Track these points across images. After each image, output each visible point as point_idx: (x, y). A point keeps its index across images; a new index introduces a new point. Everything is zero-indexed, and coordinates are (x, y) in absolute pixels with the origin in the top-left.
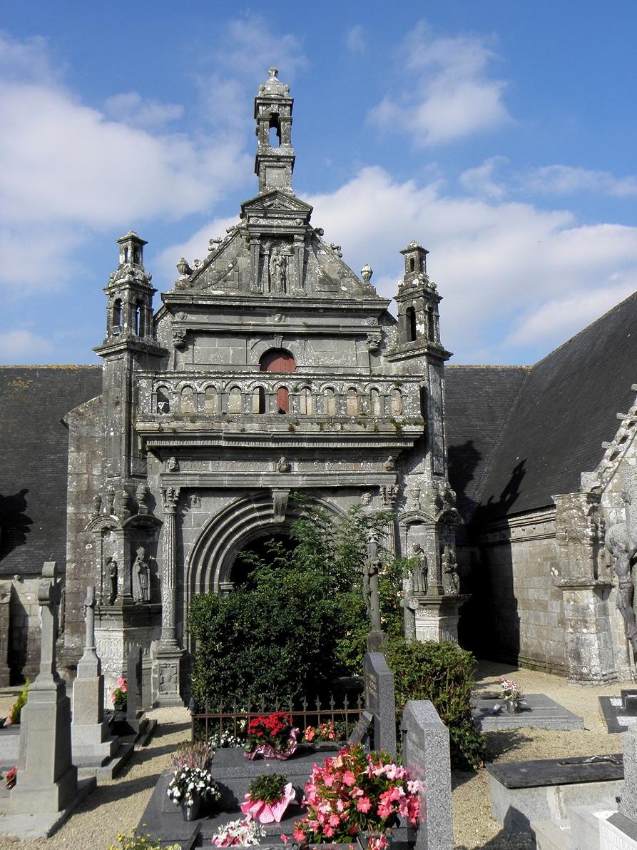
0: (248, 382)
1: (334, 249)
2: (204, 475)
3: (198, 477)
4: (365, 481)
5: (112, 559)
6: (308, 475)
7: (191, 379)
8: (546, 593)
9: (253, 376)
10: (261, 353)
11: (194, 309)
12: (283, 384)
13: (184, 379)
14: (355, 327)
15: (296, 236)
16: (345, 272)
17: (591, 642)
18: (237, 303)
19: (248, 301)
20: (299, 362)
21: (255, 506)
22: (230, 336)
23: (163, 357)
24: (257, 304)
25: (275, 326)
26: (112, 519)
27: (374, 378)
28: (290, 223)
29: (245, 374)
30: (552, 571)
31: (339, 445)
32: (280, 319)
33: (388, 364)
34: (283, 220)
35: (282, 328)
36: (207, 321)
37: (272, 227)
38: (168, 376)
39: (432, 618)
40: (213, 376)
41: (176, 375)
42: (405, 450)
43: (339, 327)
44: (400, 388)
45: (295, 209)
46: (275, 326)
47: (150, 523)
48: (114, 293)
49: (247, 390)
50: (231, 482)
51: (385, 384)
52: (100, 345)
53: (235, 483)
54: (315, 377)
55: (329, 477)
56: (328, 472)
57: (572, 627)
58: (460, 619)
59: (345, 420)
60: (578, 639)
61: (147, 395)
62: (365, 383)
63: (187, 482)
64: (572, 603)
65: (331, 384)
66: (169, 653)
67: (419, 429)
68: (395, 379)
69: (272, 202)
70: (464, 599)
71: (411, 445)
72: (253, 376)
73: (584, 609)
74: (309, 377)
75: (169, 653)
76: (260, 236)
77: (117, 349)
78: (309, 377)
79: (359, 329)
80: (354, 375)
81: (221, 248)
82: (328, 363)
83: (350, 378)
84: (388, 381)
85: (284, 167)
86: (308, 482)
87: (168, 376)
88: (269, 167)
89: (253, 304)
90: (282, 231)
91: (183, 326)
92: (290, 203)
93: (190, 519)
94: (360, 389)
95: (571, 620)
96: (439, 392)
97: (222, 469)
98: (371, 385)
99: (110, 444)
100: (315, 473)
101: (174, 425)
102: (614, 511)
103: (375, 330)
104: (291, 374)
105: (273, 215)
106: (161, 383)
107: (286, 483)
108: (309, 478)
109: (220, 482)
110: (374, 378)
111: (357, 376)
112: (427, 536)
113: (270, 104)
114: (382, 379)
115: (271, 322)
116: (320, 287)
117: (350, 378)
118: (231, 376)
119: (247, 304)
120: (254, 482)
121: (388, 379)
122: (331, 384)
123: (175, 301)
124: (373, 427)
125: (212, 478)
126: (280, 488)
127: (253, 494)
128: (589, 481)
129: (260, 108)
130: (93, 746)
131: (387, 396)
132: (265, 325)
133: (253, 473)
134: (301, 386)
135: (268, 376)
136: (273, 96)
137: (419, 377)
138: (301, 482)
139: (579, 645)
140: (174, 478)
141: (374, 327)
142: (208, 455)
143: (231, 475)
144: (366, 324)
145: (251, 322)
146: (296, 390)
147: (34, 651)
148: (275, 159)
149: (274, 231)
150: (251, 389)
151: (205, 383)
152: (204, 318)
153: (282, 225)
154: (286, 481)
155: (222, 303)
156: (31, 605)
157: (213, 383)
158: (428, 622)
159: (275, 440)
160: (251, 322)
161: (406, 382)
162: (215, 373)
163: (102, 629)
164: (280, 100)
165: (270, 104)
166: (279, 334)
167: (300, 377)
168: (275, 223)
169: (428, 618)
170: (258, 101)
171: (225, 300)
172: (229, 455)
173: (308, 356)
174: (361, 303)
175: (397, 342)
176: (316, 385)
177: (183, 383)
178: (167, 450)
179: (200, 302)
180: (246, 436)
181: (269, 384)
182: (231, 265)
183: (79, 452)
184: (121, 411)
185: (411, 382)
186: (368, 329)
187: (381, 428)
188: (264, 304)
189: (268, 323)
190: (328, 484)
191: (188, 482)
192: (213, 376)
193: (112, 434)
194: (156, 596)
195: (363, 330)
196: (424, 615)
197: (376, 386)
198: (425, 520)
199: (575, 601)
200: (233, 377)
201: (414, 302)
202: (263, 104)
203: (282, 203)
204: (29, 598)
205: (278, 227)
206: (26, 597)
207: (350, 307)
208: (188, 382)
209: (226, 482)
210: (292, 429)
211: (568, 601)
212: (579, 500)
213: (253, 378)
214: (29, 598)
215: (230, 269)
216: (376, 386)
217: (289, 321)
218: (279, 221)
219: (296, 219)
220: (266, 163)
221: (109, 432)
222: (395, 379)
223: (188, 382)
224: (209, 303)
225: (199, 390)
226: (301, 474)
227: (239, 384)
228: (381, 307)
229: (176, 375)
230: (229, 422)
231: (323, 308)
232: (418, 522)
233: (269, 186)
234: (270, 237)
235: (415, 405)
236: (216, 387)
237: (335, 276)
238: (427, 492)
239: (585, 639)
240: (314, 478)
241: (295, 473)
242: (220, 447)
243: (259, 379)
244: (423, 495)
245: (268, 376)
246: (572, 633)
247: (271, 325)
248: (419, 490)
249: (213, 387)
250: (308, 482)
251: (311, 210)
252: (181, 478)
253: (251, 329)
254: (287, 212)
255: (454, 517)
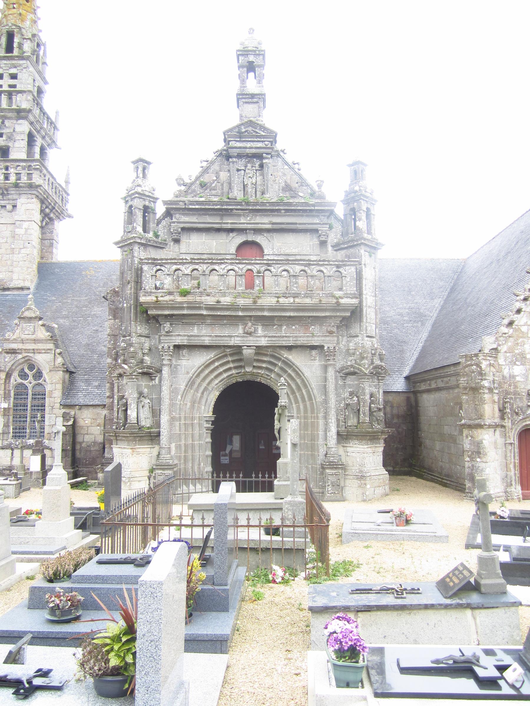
0: (223, 266)
1: (294, 164)
2: (192, 336)
3: (186, 338)
4: (313, 342)
5: (124, 396)
6: (269, 337)
7: (181, 264)
8: (456, 429)
9: (227, 261)
10: (237, 245)
11: (187, 212)
12: (249, 267)
13: (175, 264)
14: (309, 224)
15: (264, 155)
16: (303, 183)
17: (482, 469)
18: (218, 207)
19: (227, 205)
20: (266, 251)
21: (230, 359)
22: (214, 232)
23: (164, 248)
24: (233, 207)
25: (247, 224)
26: (123, 368)
27: (320, 263)
28: (260, 145)
29: (220, 260)
30: (460, 413)
31: (292, 314)
32: (250, 220)
33: (335, 252)
34: (255, 143)
35: (253, 225)
36: (196, 221)
37: (246, 148)
38: (164, 261)
39: (362, 446)
40: (196, 261)
41: (169, 261)
42: (344, 318)
43: (296, 224)
44: (340, 270)
45: (264, 134)
46: (247, 224)
47: (151, 371)
48: (128, 201)
49: (222, 272)
50: (211, 342)
51: (328, 267)
52: (119, 239)
53: (214, 342)
54: (274, 262)
55: (285, 339)
56: (284, 335)
57: (469, 457)
58: (385, 447)
59: (296, 296)
60: (473, 466)
61: (148, 276)
62: (313, 267)
63: (178, 341)
64: (470, 438)
65: (287, 267)
66: (164, 465)
67: (355, 301)
68: (336, 263)
69: (247, 129)
70: (388, 432)
71: (348, 314)
72: (227, 261)
73: (478, 443)
74: (270, 262)
75: (164, 465)
76: (238, 155)
77: (128, 242)
78: (270, 262)
79: (311, 226)
80: (304, 260)
81: (208, 165)
82: (288, 252)
83: (301, 262)
84: (331, 265)
85: (257, 102)
86: (269, 342)
87: (164, 261)
88: (246, 103)
89: (231, 207)
90: (254, 151)
91: (179, 225)
92: (260, 129)
93: (182, 368)
94: (309, 271)
95: (468, 451)
96: (374, 274)
97: (205, 331)
98: (318, 268)
99: (124, 313)
100: (274, 335)
101: (167, 298)
102: (508, 368)
103: (325, 226)
104: (256, 260)
105: (247, 139)
106: (158, 267)
107: (252, 342)
108: (270, 339)
109: (203, 342)
110: (320, 263)
111: (307, 261)
112: (360, 384)
113: (247, 55)
114: (326, 263)
115: (243, 221)
116: (283, 193)
117: (301, 262)
118: (210, 261)
119: (225, 207)
120: (227, 342)
121: (331, 263)
122: (287, 267)
123: (172, 206)
124: (318, 300)
125: (196, 338)
126: (247, 346)
127: (228, 351)
128: (488, 344)
129: (240, 58)
130: (54, 538)
131: (330, 276)
132: (240, 223)
133: (227, 335)
134: (263, 269)
135: (238, 261)
136: (249, 48)
137: (355, 261)
138: (263, 342)
139: (474, 471)
140: (169, 338)
141: (323, 224)
142: (194, 321)
143: (211, 336)
144: (318, 222)
145: (229, 222)
146: (259, 272)
147: (90, 458)
148: (250, 96)
149: (248, 151)
150: (226, 271)
151: (191, 267)
152: (194, 219)
153: (254, 146)
154: (252, 341)
155: (207, 207)
156: (88, 427)
157: (197, 267)
158: (358, 449)
159: (244, 310)
160: (229, 222)
161: (345, 265)
162: (198, 259)
163: (117, 446)
164: (255, 51)
165: (247, 55)
166: (250, 229)
167: (262, 262)
168: (249, 145)
169: (359, 446)
170: (238, 53)
171: (209, 205)
172: (209, 321)
173: (273, 246)
174: (313, 205)
175: (342, 235)
176: (274, 268)
177: (175, 267)
178: (164, 317)
179: (190, 207)
180: (221, 306)
181: (239, 268)
182: (215, 178)
183: (115, 320)
184: (131, 288)
185: (348, 265)
186: (319, 226)
187: (324, 301)
188: (239, 207)
189: (242, 221)
190: (284, 344)
191: (179, 341)
192: (196, 261)
193: (125, 305)
194: (158, 424)
195: (315, 226)
196: (355, 444)
197: (322, 268)
198: (358, 372)
199: (472, 437)
200: (148, 260)
201: (355, 204)
202: (242, 55)
203: (254, 129)
204: (87, 422)
205: (251, 148)
206: (85, 421)
207: (305, 208)
208: (178, 267)
209: (207, 341)
210: (255, 302)
211: (467, 437)
212: (478, 359)
213: (226, 263)
214: (87, 422)
215: (214, 181)
216: (322, 268)
217: (258, 220)
218: (252, 144)
219: (265, 141)
220: (243, 100)
221: (124, 303)
222: (336, 263)
223: (178, 267)
224: (197, 207)
225: (186, 272)
226: (262, 337)
227: (216, 267)
228: (329, 208)
229: (169, 261)
230: (208, 295)
231: (284, 210)
232: (354, 373)
233: (246, 117)
234: (244, 156)
235: (352, 284)
236: (199, 269)
237: (294, 185)
238: (360, 351)
239: (478, 467)
240: (273, 339)
241: (259, 335)
242: (202, 315)
243: (232, 264)
244: (358, 353)
245: (238, 261)
246: (468, 461)
247: (244, 223)
248: (355, 349)
249: (197, 269)
250: (269, 342)
251: (276, 135)
252: (174, 338)
253: (229, 226)
254: (257, 137)
255: (382, 370)
